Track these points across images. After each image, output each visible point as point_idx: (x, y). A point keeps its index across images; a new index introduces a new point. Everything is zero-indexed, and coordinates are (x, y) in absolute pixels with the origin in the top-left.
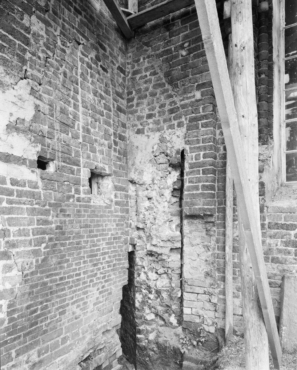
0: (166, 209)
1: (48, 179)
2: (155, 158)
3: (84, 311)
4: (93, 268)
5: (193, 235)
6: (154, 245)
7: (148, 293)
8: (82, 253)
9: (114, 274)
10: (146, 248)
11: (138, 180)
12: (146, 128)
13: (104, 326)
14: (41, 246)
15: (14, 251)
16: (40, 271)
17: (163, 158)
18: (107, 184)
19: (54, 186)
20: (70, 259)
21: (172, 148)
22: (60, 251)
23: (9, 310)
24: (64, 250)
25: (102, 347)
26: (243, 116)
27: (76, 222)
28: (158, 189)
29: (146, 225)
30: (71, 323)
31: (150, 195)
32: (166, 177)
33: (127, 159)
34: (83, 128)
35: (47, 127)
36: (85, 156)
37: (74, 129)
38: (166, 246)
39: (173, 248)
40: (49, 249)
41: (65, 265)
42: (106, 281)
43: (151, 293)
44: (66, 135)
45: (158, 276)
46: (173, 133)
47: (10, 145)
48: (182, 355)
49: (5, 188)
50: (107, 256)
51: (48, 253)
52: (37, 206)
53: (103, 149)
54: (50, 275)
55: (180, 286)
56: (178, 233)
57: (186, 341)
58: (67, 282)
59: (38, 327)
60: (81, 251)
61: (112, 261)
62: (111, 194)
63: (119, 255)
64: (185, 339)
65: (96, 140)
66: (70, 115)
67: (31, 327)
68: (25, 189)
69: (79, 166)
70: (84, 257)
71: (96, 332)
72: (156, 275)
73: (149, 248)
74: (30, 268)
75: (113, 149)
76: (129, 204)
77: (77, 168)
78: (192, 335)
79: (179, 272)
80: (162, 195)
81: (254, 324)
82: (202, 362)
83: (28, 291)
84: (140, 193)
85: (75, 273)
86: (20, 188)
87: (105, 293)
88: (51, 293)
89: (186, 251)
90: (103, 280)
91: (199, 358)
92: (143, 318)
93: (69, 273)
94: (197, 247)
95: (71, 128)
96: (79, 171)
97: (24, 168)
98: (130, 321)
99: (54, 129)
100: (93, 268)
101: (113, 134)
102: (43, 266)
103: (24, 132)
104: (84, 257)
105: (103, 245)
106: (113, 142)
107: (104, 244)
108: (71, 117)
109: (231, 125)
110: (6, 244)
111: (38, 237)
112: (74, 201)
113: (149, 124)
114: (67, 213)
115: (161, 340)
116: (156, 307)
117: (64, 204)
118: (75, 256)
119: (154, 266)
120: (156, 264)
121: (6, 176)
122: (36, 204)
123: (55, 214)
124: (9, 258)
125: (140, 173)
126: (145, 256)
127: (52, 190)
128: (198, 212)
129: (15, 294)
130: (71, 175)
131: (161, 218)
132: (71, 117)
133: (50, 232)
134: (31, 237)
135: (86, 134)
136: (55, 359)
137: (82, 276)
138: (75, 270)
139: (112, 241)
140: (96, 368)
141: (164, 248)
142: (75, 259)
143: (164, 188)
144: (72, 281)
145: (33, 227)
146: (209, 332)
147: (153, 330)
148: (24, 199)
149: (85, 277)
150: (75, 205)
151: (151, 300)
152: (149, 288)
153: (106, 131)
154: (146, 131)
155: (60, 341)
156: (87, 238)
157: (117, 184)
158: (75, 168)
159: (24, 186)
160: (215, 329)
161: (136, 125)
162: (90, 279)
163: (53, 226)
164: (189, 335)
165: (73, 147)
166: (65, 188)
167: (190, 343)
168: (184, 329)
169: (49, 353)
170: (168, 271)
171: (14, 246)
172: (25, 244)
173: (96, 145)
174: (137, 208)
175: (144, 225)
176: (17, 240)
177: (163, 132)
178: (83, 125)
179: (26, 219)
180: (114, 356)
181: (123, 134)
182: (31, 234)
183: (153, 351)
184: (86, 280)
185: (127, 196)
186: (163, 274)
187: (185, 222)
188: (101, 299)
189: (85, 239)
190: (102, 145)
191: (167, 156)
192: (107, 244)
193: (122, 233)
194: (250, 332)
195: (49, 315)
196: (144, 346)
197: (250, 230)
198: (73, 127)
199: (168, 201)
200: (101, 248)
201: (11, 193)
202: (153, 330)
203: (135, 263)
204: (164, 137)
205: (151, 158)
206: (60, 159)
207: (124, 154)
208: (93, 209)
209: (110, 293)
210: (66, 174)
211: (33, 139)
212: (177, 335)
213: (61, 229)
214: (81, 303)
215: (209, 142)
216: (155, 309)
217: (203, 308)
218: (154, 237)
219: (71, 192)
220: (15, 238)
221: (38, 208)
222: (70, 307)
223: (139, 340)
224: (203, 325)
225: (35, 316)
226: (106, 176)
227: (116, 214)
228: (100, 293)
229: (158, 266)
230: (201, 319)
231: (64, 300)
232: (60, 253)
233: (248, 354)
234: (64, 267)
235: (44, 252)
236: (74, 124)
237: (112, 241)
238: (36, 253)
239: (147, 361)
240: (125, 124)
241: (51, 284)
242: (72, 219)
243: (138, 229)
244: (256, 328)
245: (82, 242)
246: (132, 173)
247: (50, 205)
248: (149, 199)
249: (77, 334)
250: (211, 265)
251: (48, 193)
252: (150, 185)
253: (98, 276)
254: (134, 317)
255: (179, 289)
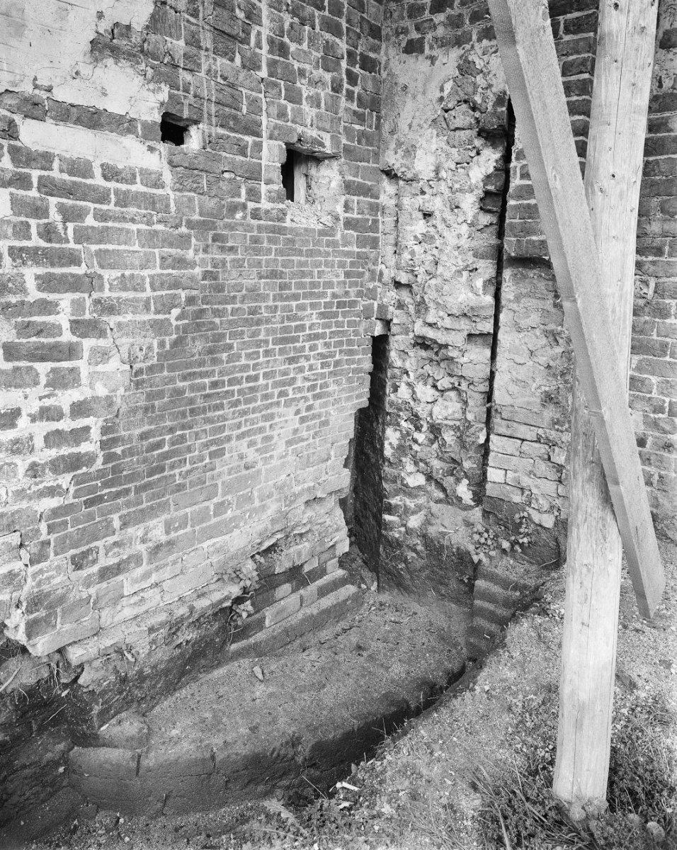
0: (464, 242)
1: (185, 165)
2: (446, 115)
3: (265, 455)
4: (287, 366)
5: (522, 305)
6: (430, 325)
7: (413, 429)
8: (263, 333)
9: (337, 383)
10: (413, 331)
11: (403, 169)
12: (429, 36)
13: (309, 489)
14: (170, 313)
15: (112, 320)
16: (169, 365)
17: (463, 114)
18: (329, 177)
19: (199, 183)
20: (235, 345)
21: (487, 88)
22: (213, 326)
23: (104, 438)
24: (221, 324)
25: (303, 531)
26: (616, 6)
27: (250, 265)
28: (447, 192)
29: (416, 276)
30: (235, 475)
31: (429, 207)
32: (468, 163)
33: (379, 118)
34: (271, 42)
35: (182, 43)
36: (273, 110)
37: (248, 44)
38: (457, 327)
39: (473, 332)
40: (187, 321)
41: (224, 356)
42: (316, 397)
43: (420, 431)
44: (228, 62)
45: (437, 394)
46: (494, 49)
47: (99, 88)
48: (476, 567)
49: (90, 185)
50: (320, 342)
51: (185, 329)
52: (160, 227)
53: (318, 95)
54: (190, 374)
55: (484, 420)
56: (489, 299)
57: (486, 539)
58: (227, 392)
59: (166, 477)
60: (260, 330)
61: (332, 355)
62: (337, 201)
63: (350, 342)
64: (486, 535)
65: (302, 73)
66: (237, 11)
67: (151, 476)
68: (133, 188)
69: (258, 135)
70: (266, 342)
71: (291, 500)
72: (433, 391)
73: (420, 329)
74: (146, 358)
75: (344, 92)
76: (381, 226)
77: (254, 141)
78: (503, 528)
79: (484, 387)
80: (457, 207)
81: (591, 515)
82: (516, 584)
83: (142, 403)
84: (406, 201)
85: (245, 375)
86: (123, 187)
87: (313, 422)
88: (192, 411)
89: (502, 341)
90: (310, 395)
91: (511, 577)
92: (399, 482)
93: (232, 373)
94: (529, 334)
95: (241, 42)
96: (258, 146)
97: (130, 142)
98: (373, 485)
99: (200, 48)
100: (287, 366)
101: (346, 57)
102: (174, 354)
103: (130, 56)
104: (266, 342)
105: (312, 318)
106: (344, 77)
107: (314, 316)
108: (240, 14)
109: (519, 37)
110: (95, 306)
111: (164, 293)
112: (244, 218)
113: (435, 27)
114: (229, 244)
115: (432, 531)
116: (428, 460)
117: (222, 224)
118: (247, 339)
119: (430, 372)
120: (435, 368)
121: (91, 159)
122: (159, 222)
123: (201, 245)
124: (102, 334)
125: (407, 151)
126: (410, 347)
127: (195, 191)
128: (537, 251)
129: (116, 409)
130: (240, 158)
131: (451, 263)
132: (240, 14)
133: (191, 284)
134: (149, 293)
135: (277, 58)
136: (201, 542)
137: (261, 381)
138: (245, 368)
139: (334, 309)
140: (290, 569)
141: (454, 332)
142: (245, 345)
143: (461, 190)
144: (239, 391)
145: (152, 272)
146: (541, 526)
147: (419, 508)
148: (132, 210)
149: (267, 384)
150: (248, 225)
151: (419, 445)
152: (415, 419)
153: (328, 48)
154: (427, 47)
155: (212, 508)
156: (274, 300)
157: (351, 178)
158: (249, 139)
159: (132, 181)
160: (554, 519)
161: (405, 31)
162: (280, 389)
163: (198, 271)
164: (496, 528)
165: (244, 91)
166: (224, 186)
167: (495, 545)
168: (486, 514)
169: (189, 529)
170: (459, 385)
171: (111, 309)
172: (136, 307)
173: (302, 86)
174: (398, 236)
175: (410, 276)
176: (119, 298)
177: (468, 47)
178: (271, 34)
179: (136, 255)
180: (331, 551)
181: (372, 55)
182: (148, 286)
183: (415, 551)
184: (270, 390)
185: (375, 208)
186: (449, 390)
187: (507, 273)
188: (304, 434)
189: (271, 303)
190: (315, 83)
191: (474, 109)
192: (323, 315)
193: (360, 294)
194: (581, 531)
195: (188, 456)
196: (397, 540)
197: (575, 301)
198: (246, 41)
199: (469, 222)
200: (308, 323)
201: (103, 197)
202: (419, 508)
203: (388, 359)
204: (470, 59)
205: (436, 116)
206: (214, 120)
207: (374, 105)
208: (289, 236)
209: (325, 423)
210: (228, 155)
211: (150, 72)
212: (469, 524)
213: (215, 279)
214: (259, 437)
215: (582, 72)
216: (426, 464)
217: (531, 472)
218: (431, 305)
219: (239, 196)
220: (114, 295)
221: (163, 232)
222: (233, 443)
223: (388, 526)
224: (527, 508)
225: (159, 455)
226: (326, 158)
227: (346, 249)
228: (303, 420)
229: (438, 373)
230: (525, 495)
231: (220, 427)
232: (213, 329)
233: (571, 576)
234: (220, 361)
235: (177, 327)
236: (249, 34)
237: (334, 309)
238: (159, 327)
239: (401, 569)
240: (379, 29)
241: (193, 395)
242: (240, 256)
243: (398, 285)
244: (594, 523)
245: (263, 308)
246: (390, 153)
247: (190, 225)
248: (427, 215)
249: (249, 499)
250: (559, 378)
251: (185, 199)
252: (431, 183)
253: (299, 383)
254: (381, 478)
255: (483, 425)
